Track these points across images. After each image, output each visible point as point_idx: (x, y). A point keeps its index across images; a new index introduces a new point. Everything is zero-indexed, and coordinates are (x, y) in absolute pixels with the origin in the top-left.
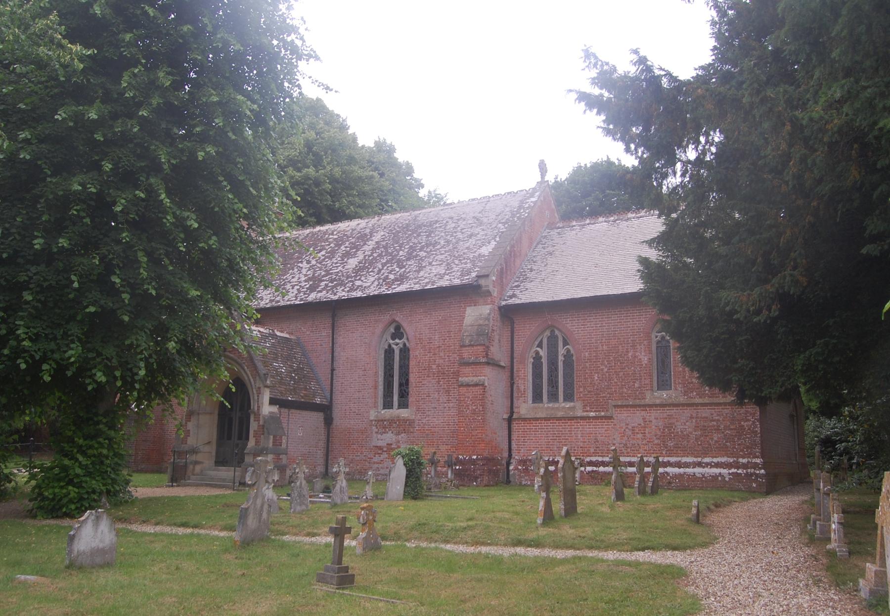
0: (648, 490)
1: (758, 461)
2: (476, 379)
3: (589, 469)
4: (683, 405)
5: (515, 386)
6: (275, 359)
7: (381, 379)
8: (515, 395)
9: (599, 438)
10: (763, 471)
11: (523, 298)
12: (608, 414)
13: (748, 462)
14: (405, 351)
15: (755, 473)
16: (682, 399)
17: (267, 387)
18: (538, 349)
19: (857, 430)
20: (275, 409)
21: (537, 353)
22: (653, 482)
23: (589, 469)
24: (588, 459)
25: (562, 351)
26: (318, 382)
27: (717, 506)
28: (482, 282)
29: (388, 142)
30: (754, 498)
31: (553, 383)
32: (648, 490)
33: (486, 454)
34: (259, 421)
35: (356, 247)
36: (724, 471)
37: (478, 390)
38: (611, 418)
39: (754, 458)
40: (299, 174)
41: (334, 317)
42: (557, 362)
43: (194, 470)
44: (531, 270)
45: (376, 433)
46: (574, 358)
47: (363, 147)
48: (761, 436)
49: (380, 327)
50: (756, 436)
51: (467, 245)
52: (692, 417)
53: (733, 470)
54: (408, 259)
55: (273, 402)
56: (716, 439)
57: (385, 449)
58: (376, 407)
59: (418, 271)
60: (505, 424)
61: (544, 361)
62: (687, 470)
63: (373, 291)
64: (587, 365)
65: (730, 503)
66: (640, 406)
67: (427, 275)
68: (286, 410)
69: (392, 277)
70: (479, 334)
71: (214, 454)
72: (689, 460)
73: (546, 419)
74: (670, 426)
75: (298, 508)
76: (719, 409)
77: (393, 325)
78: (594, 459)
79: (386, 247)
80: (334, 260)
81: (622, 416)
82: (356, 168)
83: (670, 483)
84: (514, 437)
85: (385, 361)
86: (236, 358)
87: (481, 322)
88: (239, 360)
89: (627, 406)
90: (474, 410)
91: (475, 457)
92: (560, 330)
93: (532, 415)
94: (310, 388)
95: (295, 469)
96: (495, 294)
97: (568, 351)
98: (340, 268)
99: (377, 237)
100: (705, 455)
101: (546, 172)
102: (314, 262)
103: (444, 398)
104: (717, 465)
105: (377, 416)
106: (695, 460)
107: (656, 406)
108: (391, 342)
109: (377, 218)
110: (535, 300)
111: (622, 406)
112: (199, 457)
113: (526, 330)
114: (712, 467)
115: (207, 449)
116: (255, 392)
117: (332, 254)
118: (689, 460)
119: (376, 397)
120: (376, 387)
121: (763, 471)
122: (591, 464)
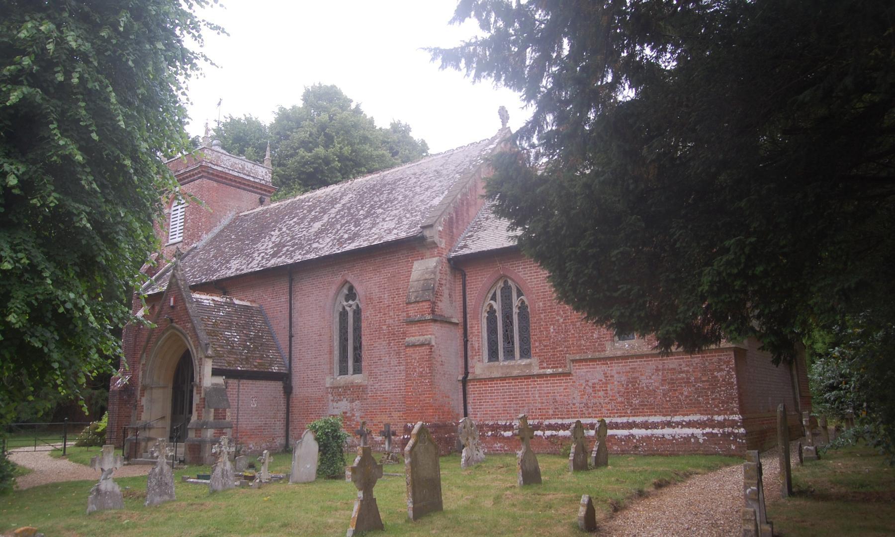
0: (591, 460)
1: (736, 417)
2: (422, 339)
3: (548, 433)
5: (469, 343)
6: (229, 328)
7: (336, 344)
8: (469, 353)
10: (742, 430)
11: (475, 247)
12: (567, 370)
13: (725, 419)
14: (358, 312)
15: (733, 433)
17: (207, 357)
18: (492, 302)
19: (851, 375)
20: (220, 380)
21: (491, 307)
22: (598, 451)
23: (548, 433)
24: (547, 422)
25: (516, 302)
26: (278, 350)
27: (659, 485)
28: (427, 233)
30: (728, 465)
31: (509, 339)
32: (591, 460)
33: (435, 420)
35: (324, 211)
36: (698, 432)
37: (424, 350)
38: (569, 374)
39: (731, 414)
41: (291, 281)
42: (512, 315)
43: (146, 447)
44: (487, 219)
47: (380, 129)
48: (739, 388)
49: (333, 289)
50: (732, 388)
51: (421, 198)
52: (657, 370)
53: (708, 430)
54: (365, 218)
55: (216, 372)
56: (686, 393)
58: (332, 373)
59: (370, 229)
60: (460, 386)
61: (499, 315)
62: (655, 431)
63: (326, 252)
65: (687, 475)
66: (600, 359)
67: (378, 231)
68: (236, 381)
69: (346, 236)
70: (425, 289)
71: (168, 429)
72: (657, 419)
73: (502, 379)
74: (634, 381)
75: (157, 499)
77: (347, 286)
78: (553, 422)
79: (349, 209)
80: (302, 226)
81: (581, 371)
83: (636, 447)
84: (470, 400)
85: (340, 322)
86: (181, 328)
87: (427, 276)
88: (184, 331)
89: (586, 360)
90: (421, 373)
92: (513, 280)
93: (487, 375)
95: (152, 453)
96: (443, 245)
97: (523, 302)
98: (304, 233)
99: (345, 200)
100: (675, 412)
101: (508, 118)
102: (284, 229)
103: (394, 362)
104: (689, 424)
105: (333, 382)
106: (664, 419)
107: (618, 358)
108: (345, 303)
109: (350, 182)
112: (151, 434)
114: (683, 426)
115: (160, 424)
117: (302, 219)
118: (657, 419)
119: (331, 363)
120: (331, 352)
121: (742, 430)
122: (550, 427)
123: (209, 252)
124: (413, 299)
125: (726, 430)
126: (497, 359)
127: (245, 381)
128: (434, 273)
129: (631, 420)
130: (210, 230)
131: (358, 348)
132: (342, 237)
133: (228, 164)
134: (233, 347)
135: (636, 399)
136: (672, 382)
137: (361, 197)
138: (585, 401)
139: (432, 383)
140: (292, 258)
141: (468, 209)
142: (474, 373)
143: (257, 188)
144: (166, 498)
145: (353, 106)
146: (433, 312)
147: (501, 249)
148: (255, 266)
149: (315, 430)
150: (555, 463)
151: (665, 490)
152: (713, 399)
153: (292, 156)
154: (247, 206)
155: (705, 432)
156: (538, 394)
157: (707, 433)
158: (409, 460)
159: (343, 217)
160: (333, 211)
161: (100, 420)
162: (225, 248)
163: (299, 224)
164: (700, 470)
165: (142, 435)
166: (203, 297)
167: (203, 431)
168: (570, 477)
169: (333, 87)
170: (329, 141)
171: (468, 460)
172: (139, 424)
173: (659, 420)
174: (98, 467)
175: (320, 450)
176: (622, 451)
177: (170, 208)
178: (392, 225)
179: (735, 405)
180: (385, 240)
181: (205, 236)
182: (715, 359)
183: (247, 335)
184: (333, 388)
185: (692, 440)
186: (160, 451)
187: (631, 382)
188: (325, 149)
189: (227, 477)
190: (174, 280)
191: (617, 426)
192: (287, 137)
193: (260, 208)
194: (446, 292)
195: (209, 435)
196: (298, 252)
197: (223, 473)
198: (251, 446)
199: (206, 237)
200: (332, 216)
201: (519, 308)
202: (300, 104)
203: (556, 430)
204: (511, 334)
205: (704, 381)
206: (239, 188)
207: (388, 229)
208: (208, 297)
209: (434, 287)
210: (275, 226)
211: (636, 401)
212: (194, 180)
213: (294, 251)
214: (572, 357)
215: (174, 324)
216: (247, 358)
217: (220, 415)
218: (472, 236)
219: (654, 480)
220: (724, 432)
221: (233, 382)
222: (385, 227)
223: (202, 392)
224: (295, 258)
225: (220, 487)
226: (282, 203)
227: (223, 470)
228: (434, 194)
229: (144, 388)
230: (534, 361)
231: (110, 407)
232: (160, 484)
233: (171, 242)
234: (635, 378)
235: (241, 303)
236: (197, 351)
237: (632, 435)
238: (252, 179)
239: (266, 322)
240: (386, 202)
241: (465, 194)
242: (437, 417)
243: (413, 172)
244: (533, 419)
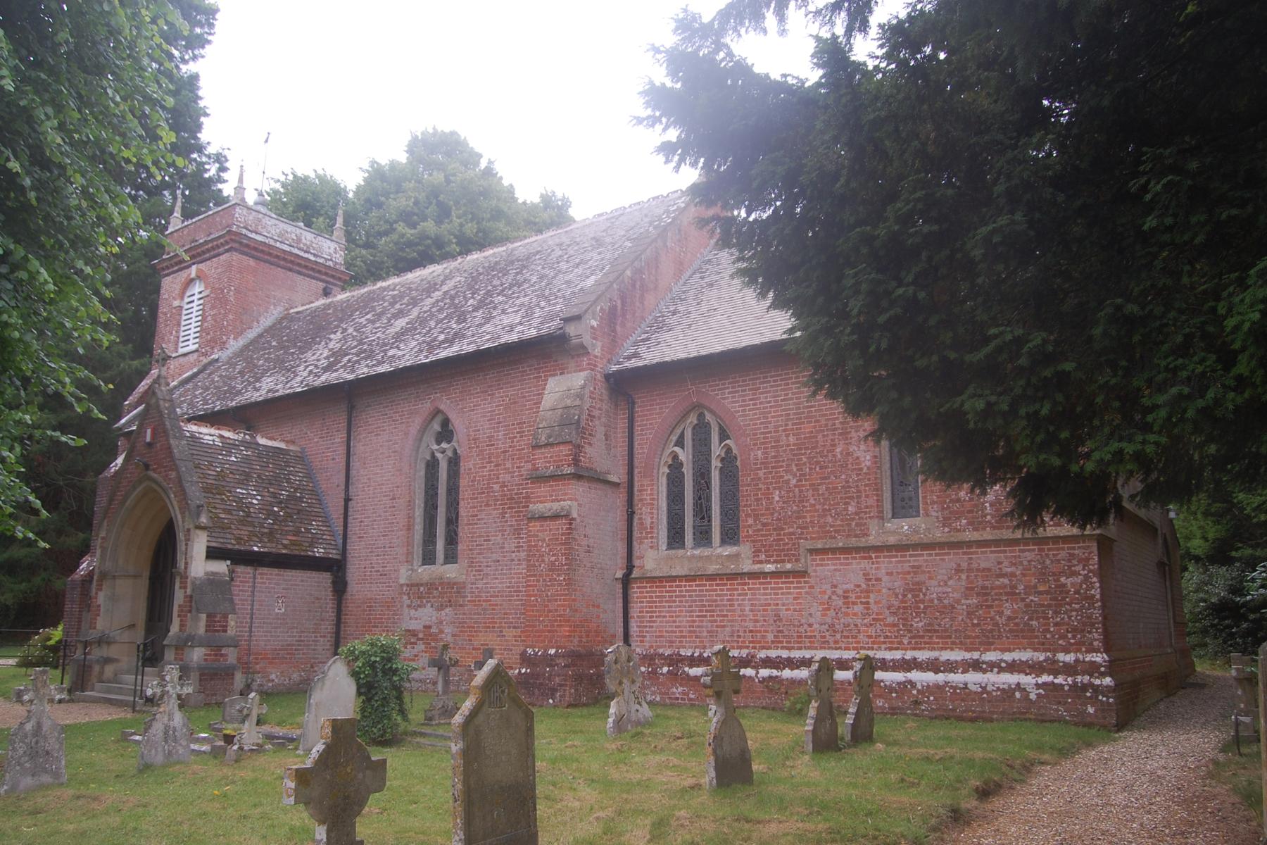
1: (1098, 658)
2: (556, 506)
3: (764, 673)
4: (942, 545)
5: (636, 517)
6: (244, 483)
7: (419, 513)
8: (636, 534)
9: (783, 613)
10: (1108, 681)
11: (650, 357)
12: (799, 566)
13: (1077, 661)
14: (454, 462)
15: (1091, 685)
16: (939, 535)
17: (198, 527)
18: (677, 449)
20: (221, 567)
21: (675, 457)
22: (857, 714)
23: (764, 673)
24: (762, 654)
25: (717, 450)
26: (327, 521)
27: (985, 793)
28: (571, 330)
29: (559, 195)
30: (1089, 745)
31: (702, 512)
33: (574, 645)
34: (185, 588)
35: (415, 302)
36: (1027, 680)
37: (559, 526)
38: (803, 574)
39: (1088, 651)
40: (413, 231)
41: (351, 409)
42: (709, 472)
43: (101, 673)
44: (674, 313)
45: (409, 606)
46: (738, 463)
47: (524, 203)
48: (1103, 607)
49: (417, 422)
50: (1092, 605)
51: (567, 278)
52: (958, 570)
53: (1045, 678)
54: (476, 309)
55: (212, 554)
56: (1008, 613)
57: (421, 636)
59: (481, 325)
60: (619, 588)
61: (688, 471)
64: (761, 473)
65: (1028, 768)
66: (857, 549)
68: (249, 569)
69: (442, 337)
70: (564, 424)
72: (956, 655)
73: (689, 578)
74: (916, 589)
75: (28, 781)
76: (958, 537)
77: (439, 419)
78: (773, 654)
79: (452, 298)
81: (824, 569)
82: (501, 225)
83: (917, 703)
84: (634, 612)
87: (569, 402)
89: (833, 550)
91: (552, 651)
93: (665, 572)
94: (308, 531)
96: (597, 352)
97: (729, 450)
100: (987, 645)
102: (350, 330)
103: (510, 544)
104: (1013, 667)
105: (410, 576)
106: (967, 656)
107: (890, 548)
108: (435, 447)
109: (460, 260)
110: (667, 359)
111: (824, 551)
112: (112, 652)
113: (655, 414)
114: (1001, 670)
115: (126, 636)
118: (956, 655)
119: (409, 544)
120: (410, 527)
122: (768, 663)
123: (233, 366)
124: (543, 440)
125: (1079, 679)
126: (682, 546)
127: (265, 570)
128: (580, 396)
129: (909, 655)
130: (241, 333)
131: (452, 521)
132: (434, 339)
133: (274, 232)
134: (248, 514)
135: (919, 619)
136: (984, 593)
137: (473, 281)
138: (829, 620)
139: (569, 582)
140: (353, 372)
141: (642, 296)
142: (642, 567)
143: (319, 272)
144: (46, 779)
145: (483, 164)
146: (576, 462)
147: (695, 358)
148: (296, 386)
149: (352, 657)
150: (776, 731)
151: (996, 803)
152: (1056, 624)
153: (386, 233)
154: (305, 298)
155: (1040, 680)
156: (749, 604)
157: (1045, 684)
158: (460, 745)
159: (441, 310)
160: (429, 301)
161: (55, 626)
162: (259, 359)
163: (373, 322)
164: (1046, 757)
165: (96, 653)
166: (204, 430)
168: (806, 768)
169: (453, 133)
170: (444, 213)
171: (619, 721)
172: (93, 635)
173: (959, 658)
174: (1025, 563)
175: (359, 693)
176: (892, 708)
177: (182, 298)
178: (516, 319)
179: (1096, 636)
180: (502, 341)
181: (232, 342)
182: (1063, 554)
183: (274, 495)
184: (411, 586)
185: (1018, 695)
186: (36, 691)
187: (912, 590)
188: (428, 216)
189: (175, 740)
191: (885, 665)
192: (379, 205)
193: (322, 302)
194: (600, 431)
195: (195, 658)
196: (364, 363)
197: (166, 733)
198: (273, 676)
199: (234, 345)
200: (425, 309)
201: (722, 460)
202: (403, 158)
203: (777, 668)
204: (709, 502)
205: (1041, 593)
206: (290, 270)
207: (510, 325)
208: (212, 431)
209: (578, 421)
210: (338, 326)
211: (918, 624)
212: (219, 255)
213: (358, 362)
214: (809, 544)
215: (151, 473)
216: (271, 533)
217: (216, 624)
218: (648, 339)
219: (975, 783)
220: (1075, 683)
221: (243, 571)
222: (505, 322)
223: (189, 585)
224: (359, 372)
225: (160, 759)
226: (355, 293)
227: (167, 728)
228: (588, 272)
230: (745, 549)
232: (33, 753)
233: (181, 351)
234: (918, 583)
235: (270, 443)
236: (183, 518)
237: (910, 682)
238: (312, 258)
239: (309, 476)
240: (511, 286)
241: (639, 271)
242: (576, 641)
243: (557, 241)
244: (740, 648)
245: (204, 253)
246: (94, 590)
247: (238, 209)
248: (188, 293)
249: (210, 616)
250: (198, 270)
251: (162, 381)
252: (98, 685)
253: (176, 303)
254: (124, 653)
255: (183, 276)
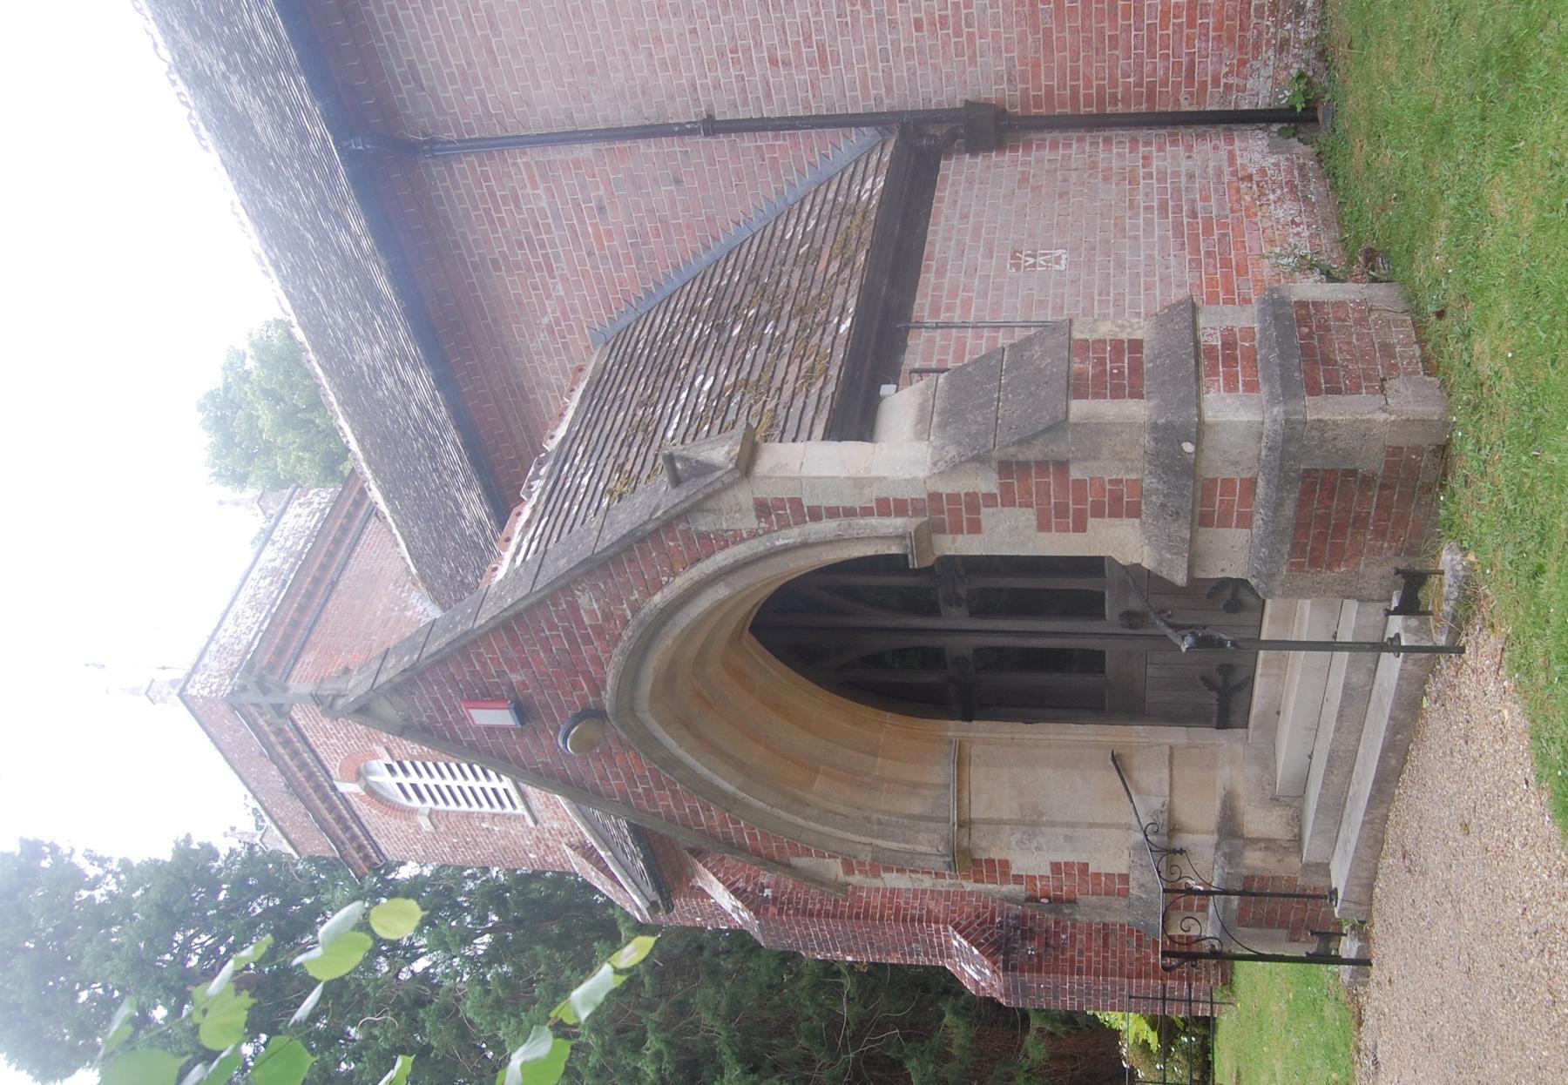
17: (746, 463)
20: (900, 406)
34: (974, 502)
43: (1269, 844)
71: (1177, 736)
86: (617, 656)
115: (1151, 778)
116: (792, 536)
161: (1115, 1034)
165: (1204, 864)
167: (1217, 466)
172: (1146, 883)
190: (386, 709)
206: (334, 584)
221: (917, 350)
229: (964, 860)
231: (1070, 1003)
245: (303, 765)
246: (1010, 888)
247: (191, 691)
248: (402, 800)
249: (1078, 387)
250: (344, 779)
251: (328, 688)
252: (1311, 849)
253: (425, 824)
254: (1195, 778)
255: (366, 811)
